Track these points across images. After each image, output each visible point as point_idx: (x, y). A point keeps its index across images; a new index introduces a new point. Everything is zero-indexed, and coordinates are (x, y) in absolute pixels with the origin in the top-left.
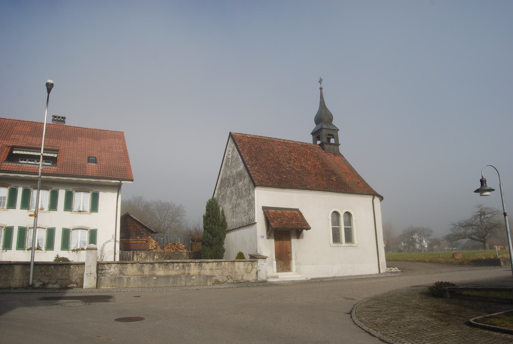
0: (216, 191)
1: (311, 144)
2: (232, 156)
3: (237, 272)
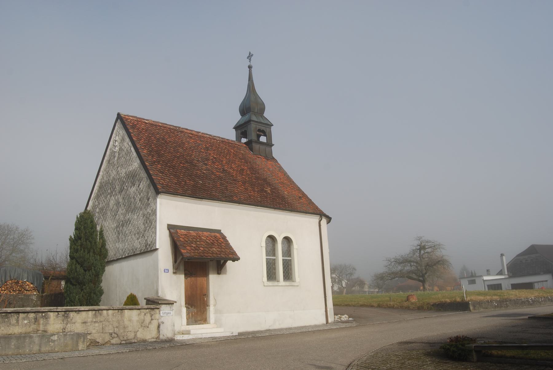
0: (90, 201)
1: (234, 141)
2: (120, 149)
3: (127, 327)
